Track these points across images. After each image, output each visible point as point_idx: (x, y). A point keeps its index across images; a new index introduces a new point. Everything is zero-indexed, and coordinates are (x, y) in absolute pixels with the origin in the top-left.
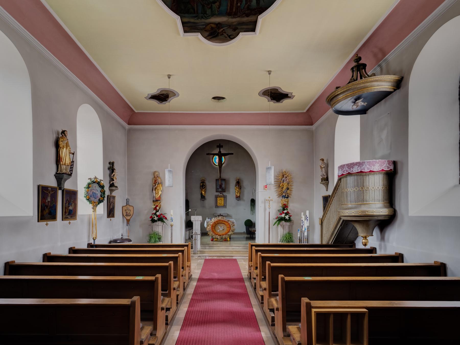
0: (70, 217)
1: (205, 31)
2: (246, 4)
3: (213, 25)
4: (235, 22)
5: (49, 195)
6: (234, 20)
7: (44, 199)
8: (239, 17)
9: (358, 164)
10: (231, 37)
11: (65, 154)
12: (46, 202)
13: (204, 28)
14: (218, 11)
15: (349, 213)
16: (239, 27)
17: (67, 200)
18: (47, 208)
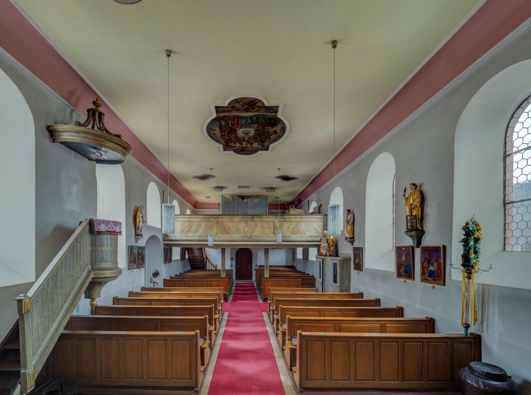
0: (431, 280)
1: (259, 107)
2: (228, 122)
3: (252, 110)
4: (234, 113)
5: (404, 254)
6: (234, 113)
7: (400, 258)
8: (231, 116)
9: (105, 223)
10: (235, 101)
12: (401, 261)
13: (260, 108)
14: (248, 119)
15: (107, 274)
16: (230, 109)
17: (426, 258)
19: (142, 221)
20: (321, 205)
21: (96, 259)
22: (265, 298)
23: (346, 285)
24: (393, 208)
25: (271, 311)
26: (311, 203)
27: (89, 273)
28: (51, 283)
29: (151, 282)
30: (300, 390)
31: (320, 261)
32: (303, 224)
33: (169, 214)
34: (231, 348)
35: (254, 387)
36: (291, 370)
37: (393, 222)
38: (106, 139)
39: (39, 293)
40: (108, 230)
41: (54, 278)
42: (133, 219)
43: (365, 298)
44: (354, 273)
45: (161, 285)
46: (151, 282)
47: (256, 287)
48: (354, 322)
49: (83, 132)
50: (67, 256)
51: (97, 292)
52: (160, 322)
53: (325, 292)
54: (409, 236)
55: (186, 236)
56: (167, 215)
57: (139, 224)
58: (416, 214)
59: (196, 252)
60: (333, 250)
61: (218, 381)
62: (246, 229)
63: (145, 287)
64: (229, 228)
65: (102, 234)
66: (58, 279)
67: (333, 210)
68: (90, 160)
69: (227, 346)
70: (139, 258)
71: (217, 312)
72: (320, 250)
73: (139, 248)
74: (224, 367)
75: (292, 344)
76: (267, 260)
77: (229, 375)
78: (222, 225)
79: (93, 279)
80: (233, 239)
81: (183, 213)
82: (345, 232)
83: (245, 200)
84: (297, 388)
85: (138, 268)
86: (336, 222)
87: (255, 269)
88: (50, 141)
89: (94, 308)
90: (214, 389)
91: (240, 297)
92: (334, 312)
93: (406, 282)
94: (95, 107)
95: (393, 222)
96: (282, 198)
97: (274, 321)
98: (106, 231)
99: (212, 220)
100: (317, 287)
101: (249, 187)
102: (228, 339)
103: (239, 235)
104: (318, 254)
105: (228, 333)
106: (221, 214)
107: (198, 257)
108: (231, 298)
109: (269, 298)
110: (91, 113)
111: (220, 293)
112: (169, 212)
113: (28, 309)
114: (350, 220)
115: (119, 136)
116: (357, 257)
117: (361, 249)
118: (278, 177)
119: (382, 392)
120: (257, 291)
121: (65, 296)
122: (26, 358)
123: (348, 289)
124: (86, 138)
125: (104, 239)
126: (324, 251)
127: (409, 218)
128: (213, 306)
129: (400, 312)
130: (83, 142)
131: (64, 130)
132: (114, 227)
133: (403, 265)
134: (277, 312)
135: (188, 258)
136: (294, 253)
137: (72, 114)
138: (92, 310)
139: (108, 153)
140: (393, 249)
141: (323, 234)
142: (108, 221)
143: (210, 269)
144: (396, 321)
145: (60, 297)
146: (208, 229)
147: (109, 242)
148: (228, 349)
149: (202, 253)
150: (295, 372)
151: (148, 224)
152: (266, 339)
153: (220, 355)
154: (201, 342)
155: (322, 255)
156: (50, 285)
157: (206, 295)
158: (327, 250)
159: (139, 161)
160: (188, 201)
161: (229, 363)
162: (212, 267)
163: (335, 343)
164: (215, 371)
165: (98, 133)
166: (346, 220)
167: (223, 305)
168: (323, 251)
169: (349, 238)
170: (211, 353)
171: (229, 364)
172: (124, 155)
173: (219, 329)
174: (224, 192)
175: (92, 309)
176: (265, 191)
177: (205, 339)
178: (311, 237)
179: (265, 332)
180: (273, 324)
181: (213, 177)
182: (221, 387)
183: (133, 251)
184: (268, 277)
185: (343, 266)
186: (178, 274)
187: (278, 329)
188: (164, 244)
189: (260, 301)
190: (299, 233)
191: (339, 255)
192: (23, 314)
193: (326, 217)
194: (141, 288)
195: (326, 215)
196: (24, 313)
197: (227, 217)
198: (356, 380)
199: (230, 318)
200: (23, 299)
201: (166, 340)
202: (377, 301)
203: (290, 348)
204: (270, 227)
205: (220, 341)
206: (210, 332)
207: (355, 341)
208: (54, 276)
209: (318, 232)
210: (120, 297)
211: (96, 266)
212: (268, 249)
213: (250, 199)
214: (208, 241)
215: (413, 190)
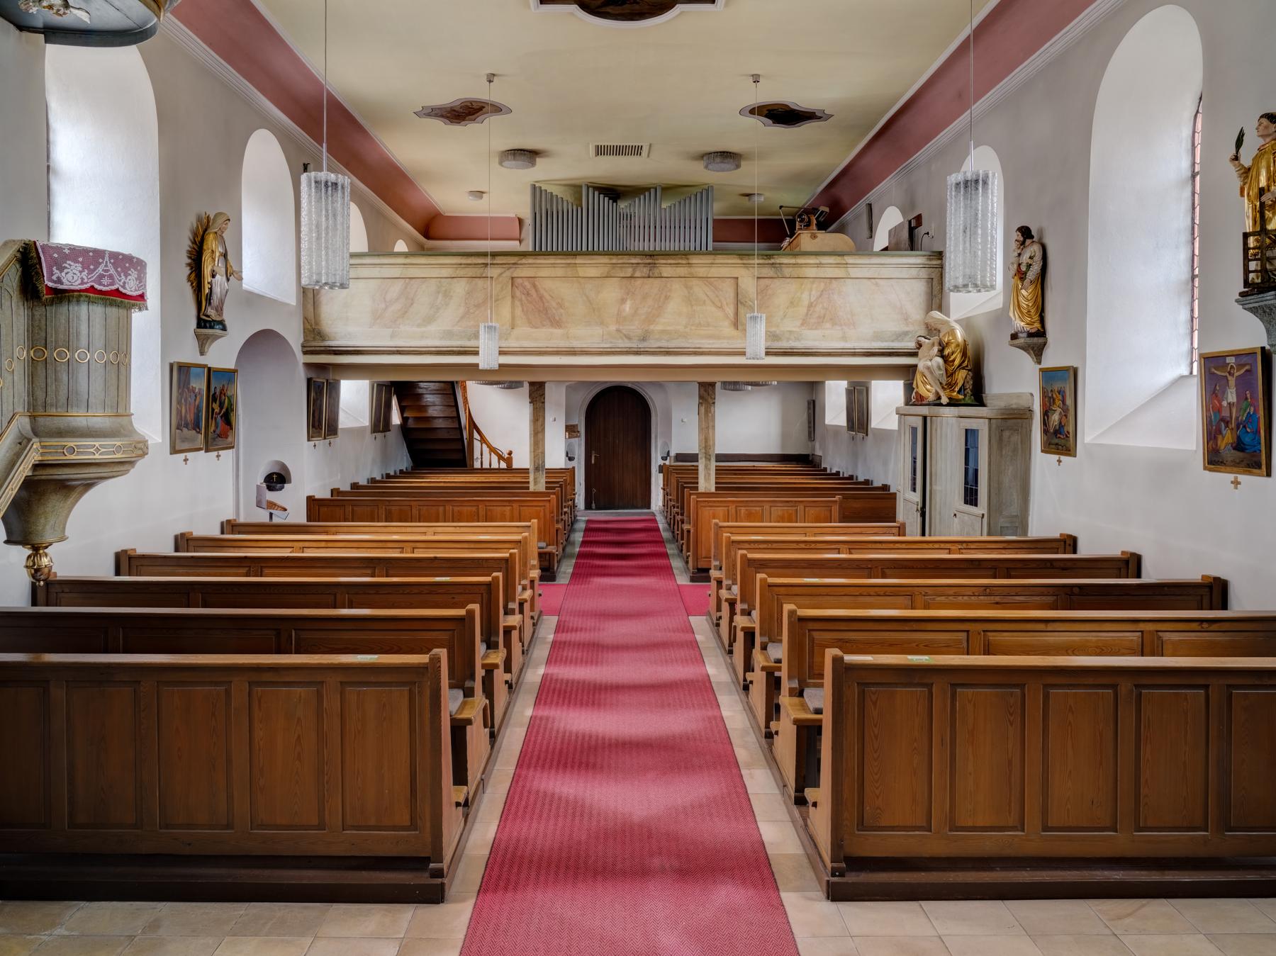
5: (1232, 381)
9: (91, 254)
15: (92, 450)
18: (1227, 426)
19: (224, 270)
20: (919, 219)
21: (49, 393)
22: (698, 569)
23: (1014, 509)
24: (1193, 219)
25: (725, 606)
26: (882, 212)
27: (20, 443)
29: (259, 505)
30: (835, 865)
31: (914, 425)
32: (849, 287)
33: (327, 211)
34: (567, 734)
35: (656, 862)
36: (800, 801)
37: (1193, 270)
40: (92, 287)
42: (189, 265)
43: (1084, 551)
44: (1042, 463)
45: (298, 515)
46: (259, 505)
47: (666, 535)
48: (1041, 627)
51: (52, 522)
52: (295, 630)
53: (930, 535)
54: (1253, 311)
55: (392, 336)
56: (319, 215)
57: (210, 283)
59: (434, 402)
60: (963, 385)
61: (518, 841)
62: (627, 307)
63: (235, 520)
64: (558, 303)
65: (69, 301)
67: (966, 192)
68: (21, 28)
69: (555, 728)
70: (213, 410)
71: (514, 605)
72: (914, 386)
74: (541, 795)
75: (804, 707)
76: (708, 428)
77: (560, 824)
78: (533, 292)
79: (36, 467)
80: (577, 344)
81: (379, 247)
82: (1011, 314)
83: (623, 205)
84: (823, 861)
85: (207, 451)
86: (979, 240)
87: (661, 469)
89: (42, 583)
90: (505, 869)
91: (602, 567)
92: (965, 598)
93: (1239, 483)
95: (1193, 270)
96: (767, 194)
97: (735, 641)
98: (86, 290)
99: (493, 272)
100: (901, 516)
101: (637, 150)
102: (557, 703)
103: (598, 331)
104: (908, 403)
105: (558, 685)
106: (531, 249)
107: (441, 420)
108: (566, 570)
109: (716, 559)
111: (525, 538)
112: (327, 205)
114: (1029, 266)
116: (1054, 403)
117: (1072, 373)
118: (752, 112)
119: (1142, 872)
120: (668, 546)
123: (1021, 522)
125: (78, 318)
126: (928, 387)
127: (1252, 242)
128: (496, 578)
129: (1215, 592)
133: (1227, 423)
134: (745, 606)
135: (401, 424)
136: (813, 409)
138: (34, 589)
140: (1191, 373)
141: (927, 325)
143: (486, 465)
144: (1201, 621)
146: (478, 306)
147: (98, 330)
148: (556, 737)
149: (456, 406)
150: (815, 805)
151: (246, 285)
152: (705, 705)
153: (525, 756)
154: (452, 702)
155: (920, 401)
157: (472, 546)
158: (941, 383)
159: (210, 45)
160: (401, 208)
161: (562, 784)
162: (495, 459)
163: (970, 691)
164: (509, 810)
166: (1015, 266)
167: (538, 590)
168: (927, 389)
169: (1025, 335)
170: (492, 747)
171: (566, 786)
173: (521, 670)
174: (542, 172)
175: (33, 585)
176: (699, 166)
177: (469, 693)
178: (878, 336)
179: (698, 681)
180: (731, 652)
181: (497, 109)
182: (531, 862)
183: (189, 384)
184: (713, 490)
185: (1001, 439)
186: (363, 482)
187: (748, 667)
188: (308, 366)
189: (683, 580)
190: (834, 321)
191: (987, 400)
193: (939, 262)
194: (222, 524)
195: (940, 255)
197: (551, 260)
198: (1046, 828)
199: (564, 637)
201: (320, 682)
202: (1126, 562)
203: (796, 722)
204: (720, 301)
205: (525, 710)
206: (490, 670)
207: (1045, 686)
209: (906, 320)
210: (141, 550)
212: (713, 385)
213: (642, 197)
214: (476, 353)
215: (1268, 140)
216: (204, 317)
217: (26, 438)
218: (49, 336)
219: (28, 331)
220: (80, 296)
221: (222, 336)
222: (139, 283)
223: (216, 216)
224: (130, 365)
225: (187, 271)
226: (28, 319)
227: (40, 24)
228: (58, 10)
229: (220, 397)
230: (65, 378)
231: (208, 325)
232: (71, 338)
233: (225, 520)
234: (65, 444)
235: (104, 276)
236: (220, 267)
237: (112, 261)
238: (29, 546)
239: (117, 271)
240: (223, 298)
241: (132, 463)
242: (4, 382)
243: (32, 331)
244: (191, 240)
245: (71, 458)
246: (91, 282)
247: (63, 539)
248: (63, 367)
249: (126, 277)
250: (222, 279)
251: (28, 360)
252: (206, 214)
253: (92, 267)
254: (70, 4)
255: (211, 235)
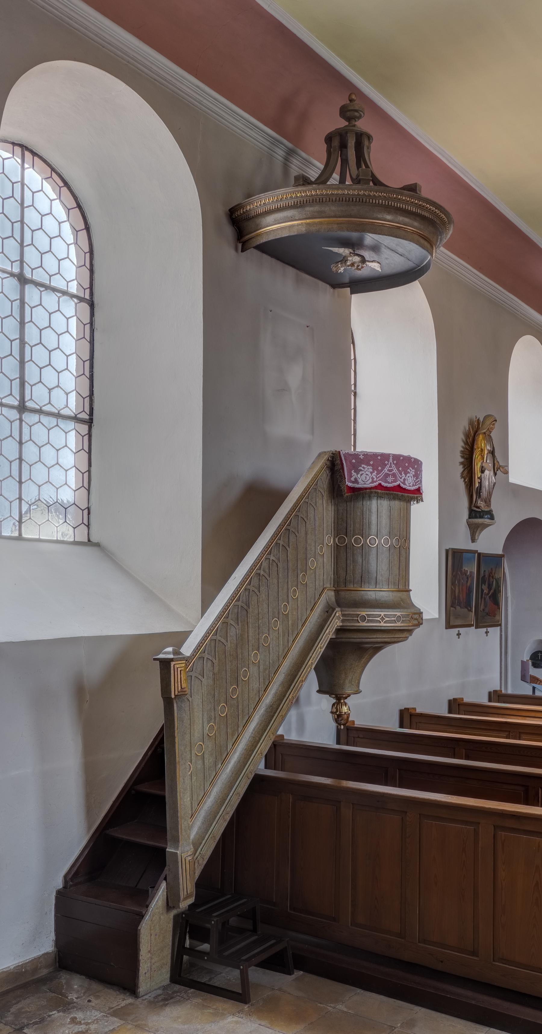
11: (158, 61)
15: (378, 619)
21: (348, 572)
27: (327, 612)
28: (233, 628)
29: (523, 678)
38: (376, 205)
39: (206, 652)
40: (380, 484)
41: (239, 616)
42: (462, 463)
46: (523, 678)
49: (313, 201)
50: (272, 558)
51: (350, 678)
57: (480, 478)
58: (360, 483)
66: (250, 620)
70: (482, 591)
73: (481, 557)
79: (339, 631)
88: (236, 250)
94: (347, 123)
98: (376, 487)
110: (336, 143)
113: (181, 688)
115: (412, 189)
121: (267, 672)
122: (178, 817)
124: (320, 215)
125: (370, 511)
130: (313, 229)
131: (267, 208)
132: (398, 475)
137: (289, 157)
138: (338, 731)
139: (383, 249)
142: (383, 455)
145: (253, 670)
147: (385, 521)
151: (513, 479)
156: (231, 634)
159: (480, 269)
165: (351, 192)
172: (428, 246)
192: (171, 698)
196: (173, 696)
200: (172, 660)
208: (239, 610)
211: (348, 593)
216: (475, 509)
217: (331, 607)
218: (349, 526)
219: (334, 523)
220: (371, 492)
221: (491, 525)
222: (416, 479)
223: (486, 417)
224: (409, 549)
225: (460, 469)
226: (334, 513)
227: (347, 280)
228: (358, 266)
229: (489, 579)
230: (360, 560)
231: (478, 516)
232: (364, 527)
233: (492, 690)
234: (359, 613)
235: (389, 475)
236: (489, 464)
237: (395, 462)
238: (334, 696)
239: (399, 470)
240: (491, 491)
241: (410, 631)
242: (317, 563)
243: (337, 522)
244: (463, 441)
245: (363, 625)
246: (379, 480)
247: (358, 692)
248: (358, 550)
249: (406, 475)
250: (490, 474)
251: (334, 546)
252: (476, 417)
253: (380, 468)
254: (367, 259)
255: (481, 436)
